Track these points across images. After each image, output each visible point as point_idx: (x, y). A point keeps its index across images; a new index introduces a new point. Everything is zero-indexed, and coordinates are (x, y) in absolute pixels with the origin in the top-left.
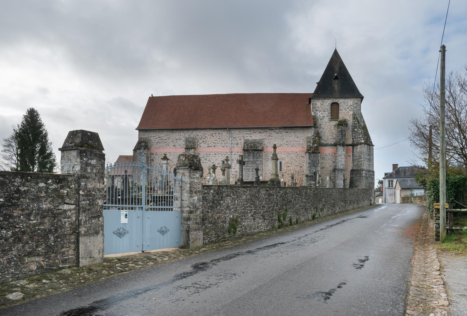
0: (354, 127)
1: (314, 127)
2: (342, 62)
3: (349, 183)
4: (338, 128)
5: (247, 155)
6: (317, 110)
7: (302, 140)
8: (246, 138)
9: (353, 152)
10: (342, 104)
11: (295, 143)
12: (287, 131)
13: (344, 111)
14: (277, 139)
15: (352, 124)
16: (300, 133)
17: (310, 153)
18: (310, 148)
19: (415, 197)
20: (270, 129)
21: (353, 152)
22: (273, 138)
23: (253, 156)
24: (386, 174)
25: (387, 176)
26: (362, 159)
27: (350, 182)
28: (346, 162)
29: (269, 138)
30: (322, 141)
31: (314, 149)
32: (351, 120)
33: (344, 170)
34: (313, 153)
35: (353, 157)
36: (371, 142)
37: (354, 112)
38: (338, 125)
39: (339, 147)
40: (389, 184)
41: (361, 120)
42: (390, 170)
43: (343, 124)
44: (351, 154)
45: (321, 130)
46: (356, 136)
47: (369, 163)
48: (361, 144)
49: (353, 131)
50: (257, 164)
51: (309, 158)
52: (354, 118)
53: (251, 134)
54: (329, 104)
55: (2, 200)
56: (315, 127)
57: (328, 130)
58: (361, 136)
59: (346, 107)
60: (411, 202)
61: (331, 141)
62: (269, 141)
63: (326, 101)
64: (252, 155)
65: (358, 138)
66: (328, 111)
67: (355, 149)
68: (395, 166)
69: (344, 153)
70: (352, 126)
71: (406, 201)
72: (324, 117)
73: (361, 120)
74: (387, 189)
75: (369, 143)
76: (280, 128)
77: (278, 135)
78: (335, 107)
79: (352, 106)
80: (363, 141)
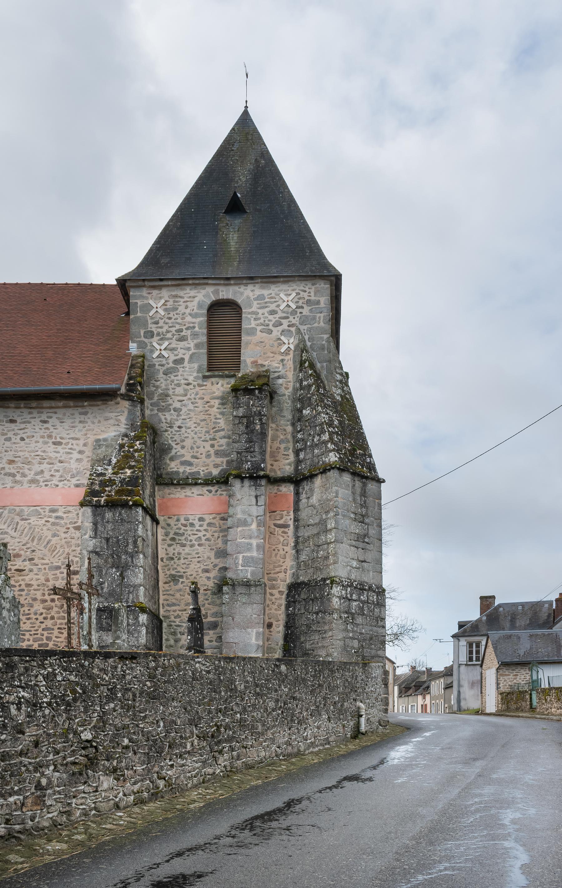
0: (301, 401)
1: (127, 397)
3: (281, 642)
4: (236, 407)
6: (150, 334)
7: (76, 455)
9: (297, 510)
11: (45, 466)
13: (260, 336)
15: (295, 390)
16: (68, 422)
17: (97, 506)
18: (103, 484)
19: (546, 692)
21: (297, 510)
24: (461, 625)
25: (465, 631)
26: (331, 537)
27: (287, 638)
28: (268, 549)
30: (174, 466)
31: (124, 496)
32: (290, 375)
33: (258, 584)
34: (112, 505)
35: (297, 528)
36: (371, 467)
38: (235, 390)
39: (237, 485)
40: (471, 652)
41: (330, 373)
42: (473, 614)
43: (255, 389)
44: (289, 519)
45: (168, 416)
46: (303, 434)
47: (360, 554)
49: (298, 418)
51: (95, 530)
52: (302, 363)
54: (200, 306)
56: (130, 399)
57: (196, 419)
58: (326, 437)
59: (272, 317)
60: (532, 709)
61: (212, 466)
63: (188, 292)
67: (303, 496)
68: (486, 602)
69: (257, 511)
70: (294, 401)
71: (514, 706)
72: (179, 361)
73: (330, 373)
74: (463, 668)
75: (358, 466)
78: (224, 317)
79: (294, 313)
80: (333, 458)
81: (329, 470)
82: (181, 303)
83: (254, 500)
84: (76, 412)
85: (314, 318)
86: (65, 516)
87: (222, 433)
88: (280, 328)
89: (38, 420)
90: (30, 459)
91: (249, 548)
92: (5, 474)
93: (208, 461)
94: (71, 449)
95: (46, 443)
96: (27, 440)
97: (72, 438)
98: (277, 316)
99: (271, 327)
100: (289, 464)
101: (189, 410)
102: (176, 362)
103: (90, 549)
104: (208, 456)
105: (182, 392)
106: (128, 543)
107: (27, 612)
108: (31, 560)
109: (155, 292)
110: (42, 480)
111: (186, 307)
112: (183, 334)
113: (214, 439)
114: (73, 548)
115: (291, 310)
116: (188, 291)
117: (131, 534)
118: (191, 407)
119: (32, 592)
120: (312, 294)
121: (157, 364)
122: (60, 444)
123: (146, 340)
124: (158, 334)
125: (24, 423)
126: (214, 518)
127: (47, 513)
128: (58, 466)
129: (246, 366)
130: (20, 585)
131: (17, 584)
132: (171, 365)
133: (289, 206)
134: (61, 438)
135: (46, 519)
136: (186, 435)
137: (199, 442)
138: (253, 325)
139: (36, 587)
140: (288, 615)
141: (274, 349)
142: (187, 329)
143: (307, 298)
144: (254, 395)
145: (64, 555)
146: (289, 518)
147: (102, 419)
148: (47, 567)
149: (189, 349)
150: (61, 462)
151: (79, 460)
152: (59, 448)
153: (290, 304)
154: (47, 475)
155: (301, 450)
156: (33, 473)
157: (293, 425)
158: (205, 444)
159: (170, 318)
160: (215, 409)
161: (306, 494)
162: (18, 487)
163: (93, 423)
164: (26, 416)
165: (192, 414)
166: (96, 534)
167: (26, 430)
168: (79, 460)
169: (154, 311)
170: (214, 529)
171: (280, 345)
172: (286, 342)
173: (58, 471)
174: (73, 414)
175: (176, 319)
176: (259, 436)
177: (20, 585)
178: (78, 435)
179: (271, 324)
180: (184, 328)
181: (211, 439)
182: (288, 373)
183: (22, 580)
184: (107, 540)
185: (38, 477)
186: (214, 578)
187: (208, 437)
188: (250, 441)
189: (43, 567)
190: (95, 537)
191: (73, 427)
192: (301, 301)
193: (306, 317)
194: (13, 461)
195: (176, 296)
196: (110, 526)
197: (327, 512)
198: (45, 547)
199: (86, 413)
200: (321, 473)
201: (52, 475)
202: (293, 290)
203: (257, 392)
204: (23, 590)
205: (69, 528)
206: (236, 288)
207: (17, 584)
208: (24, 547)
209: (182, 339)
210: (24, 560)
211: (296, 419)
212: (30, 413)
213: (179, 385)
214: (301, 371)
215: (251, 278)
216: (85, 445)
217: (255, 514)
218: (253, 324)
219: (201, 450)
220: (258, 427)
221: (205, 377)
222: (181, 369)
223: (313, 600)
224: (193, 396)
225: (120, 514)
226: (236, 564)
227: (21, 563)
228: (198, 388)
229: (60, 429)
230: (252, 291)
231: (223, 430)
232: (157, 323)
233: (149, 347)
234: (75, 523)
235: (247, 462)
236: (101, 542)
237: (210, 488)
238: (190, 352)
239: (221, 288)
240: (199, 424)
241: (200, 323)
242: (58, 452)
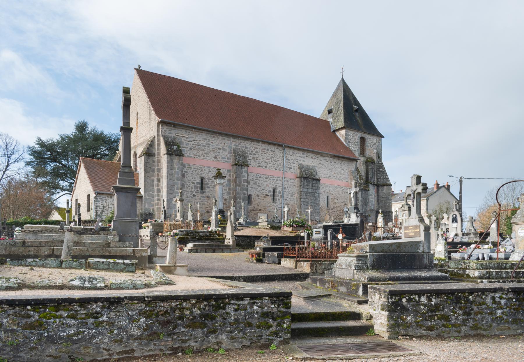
5: (306, 184)
8: (299, 162)
12: (335, 160)
20: (322, 155)
63: (356, 133)
64: (311, 184)
65: (383, 179)
77: (328, 163)
209: (355, 145)
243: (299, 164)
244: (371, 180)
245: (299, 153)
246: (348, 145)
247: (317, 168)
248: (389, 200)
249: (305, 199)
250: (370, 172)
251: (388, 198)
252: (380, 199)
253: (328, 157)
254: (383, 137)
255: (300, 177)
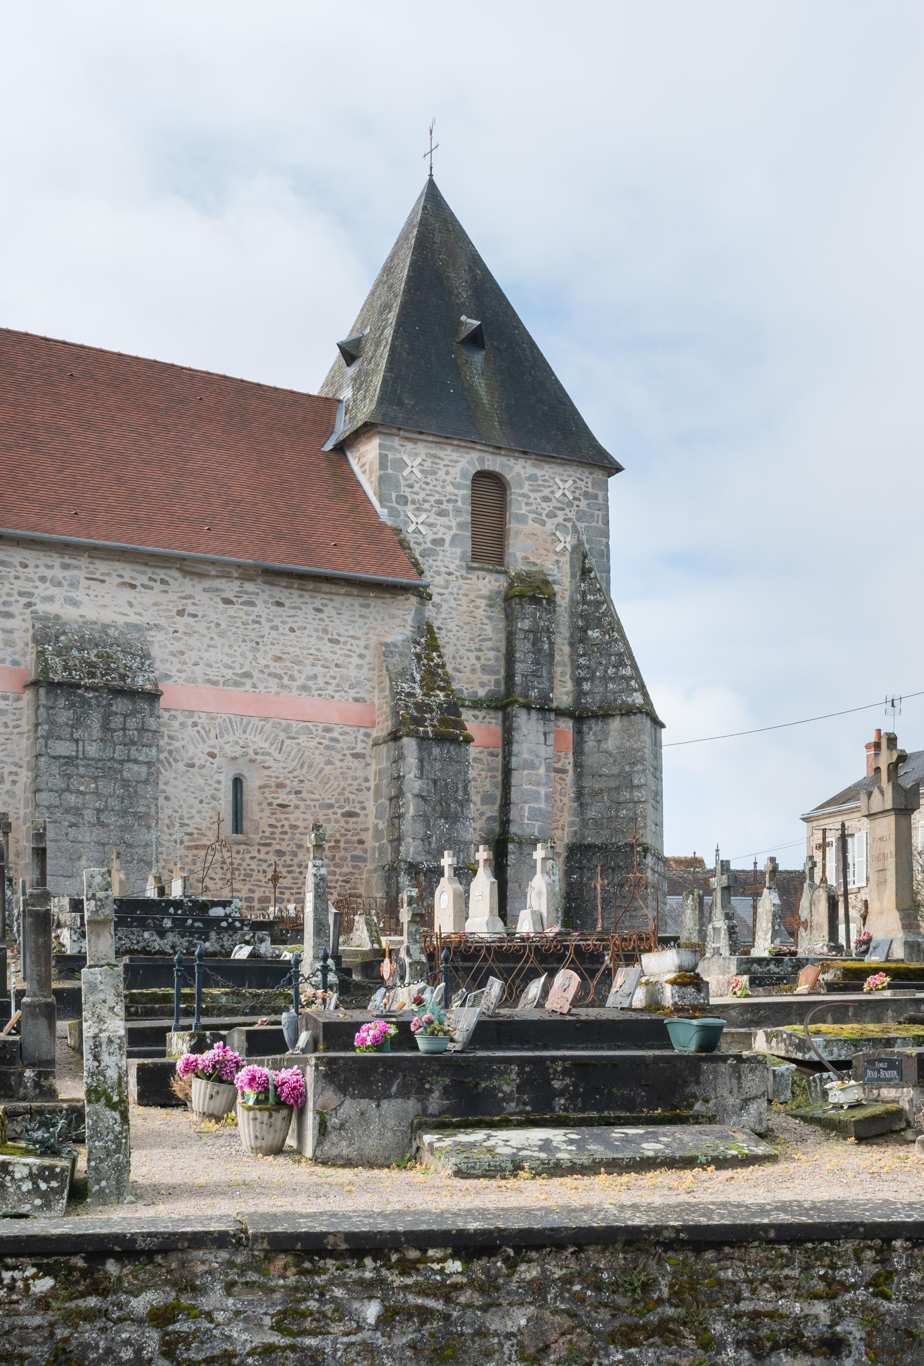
2: (476, 261)
5: (64, 716)
7: (356, 660)
8: (42, 608)
10: (526, 488)
11: (318, 670)
12: (279, 593)
14: (222, 635)
20: (189, 568)
22: (201, 627)
23: (106, 727)
29: (181, 623)
37: (580, 543)
48: (477, 704)
50: (126, 783)
53: (73, 585)
54: (463, 475)
55: (2, 1293)
62: (178, 646)
63: (449, 454)
64: (95, 720)
65: (605, 679)
66: (458, 511)
70: (572, 615)
72: (439, 542)
76: (247, 573)
77: (231, 610)
79: (569, 504)
81: (635, 714)
82: (441, 466)
83: (542, 737)
84: (357, 602)
85: (592, 516)
86: (341, 738)
87: (489, 644)
88: (555, 521)
89: (311, 607)
90: (301, 659)
91: (536, 797)
92: (270, 675)
93: (473, 677)
94: (350, 650)
95: (321, 639)
96: (298, 633)
97: (352, 637)
98: (552, 504)
99: (544, 517)
100: (567, 694)
101: (451, 608)
102: (434, 541)
103: (416, 791)
104: (473, 671)
105: (442, 583)
106: (457, 788)
107: (289, 862)
108: (298, 792)
109: (409, 445)
110: (314, 687)
111: (447, 473)
112: (443, 507)
113: (480, 650)
114: (349, 781)
115: (566, 500)
116: (449, 452)
117: (461, 777)
118: (453, 604)
119: (298, 836)
120: (590, 485)
121: (412, 541)
122: (337, 642)
123: (399, 507)
124: (413, 502)
125: (294, 608)
126: (481, 752)
127: (320, 733)
128: (333, 671)
129: (516, 561)
130: (283, 826)
131: (279, 824)
132: (429, 545)
133: (532, 352)
134: (339, 635)
135: (318, 740)
136: (447, 640)
137: (463, 651)
138: (524, 511)
139: (302, 830)
140: (570, 884)
141: (548, 546)
142: (448, 501)
143: (584, 489)
144: (541, 605)
145: (339, 790)
146: (567, 761)
147: (386, 617)
148: (317, 803)
149: (449, 528)
150: (337, 666)
151: (359, 667)
152: (336, 648)
153: (567, 492)
154: (321, 682)
155: (585, 679)
156: (303, 676)
157: (571, 645)
158: (469, 654)
159: (427, 484)
160: (481, 611)
161: (595, 734)
162: (284, 693)
163: (376, 620)
164: (297, 601)
165: (454, 613)
166: (422, 773)
167: (296, 619)
168: (359, 667)
169: (408, 470)
170: (481, 766)
171: (554, 541)
172: (562, 539)
173: (334, 678)
174: (352, 605)
175: (435, 486)
176: (548, 658)
177: (283, 826)
178: (359, 634)
179: (544, 513)
180: (444, 499)
181: (476, 650)
182: (564, 579)
183: (286, 819)
184: (435, 782)
185: (310, 683)
186: (481, 829)
187: (473, 647)
188: (536, 662)
189: (312, 803)
190: (421, 778)
191: (353, 622)
192: (578, 492)
193: (584, 512)
194: (280, 658)
195: (435, 456)
196: (437, 765)
197: (634, 764)
198: (317, 777)
199: (367, 606)
200: (622, 715)
201: (327, 683)
202: (570, 476)
203: (544, 602)
204: (285, 833)
205: (345, 755)
206: (504, 459)
207: (279, 824)
208: (291, 775)
209: (442, 514)
210: (289, 793)
211: (577, 639)
212: (301, 596)
213: (438, 573)
214: (583, 580)
215: (525, 453)
216: (366, 647)
217: (544, 755)
218: (524, 510)
219: (465, 662)
220: (546, 647)
221: (470, 569)
222: (441, 553)
223: (613, 869)
224: (455, 590)
225: (449, 751)
226: (522, 816)
227: (285, 796)
228: (461, 581)
229: (337, 622)
230: (524, 467)
231: (490, 639)
232: (411, 486)
233: (402, 517)
234: (354, 748)
235: (534, 688)
236: (428, 785)
237: (476, 712)
238: (452, 533)
239: (487, 456)
240: (462, 628)
241: (463, 497)
242: (335, 653)
243: (36, 617)
244: (527, 688)
245: (39, 564)
246: (394, 513)
247: (156, 637)
248: (632, 787)
249: (61, 792)
250: (523, 647)
251: (630, 776)
252: (587, 783)
253: (228, 576)
254: (619, 469)
255: (35, 684)
